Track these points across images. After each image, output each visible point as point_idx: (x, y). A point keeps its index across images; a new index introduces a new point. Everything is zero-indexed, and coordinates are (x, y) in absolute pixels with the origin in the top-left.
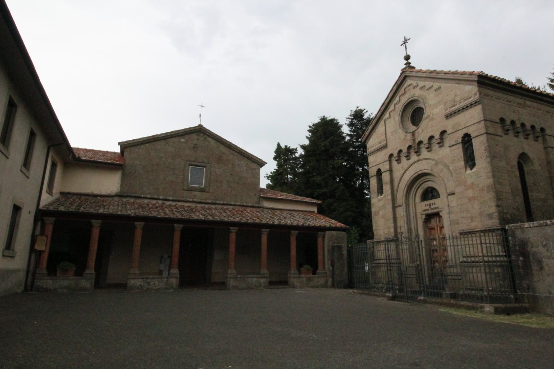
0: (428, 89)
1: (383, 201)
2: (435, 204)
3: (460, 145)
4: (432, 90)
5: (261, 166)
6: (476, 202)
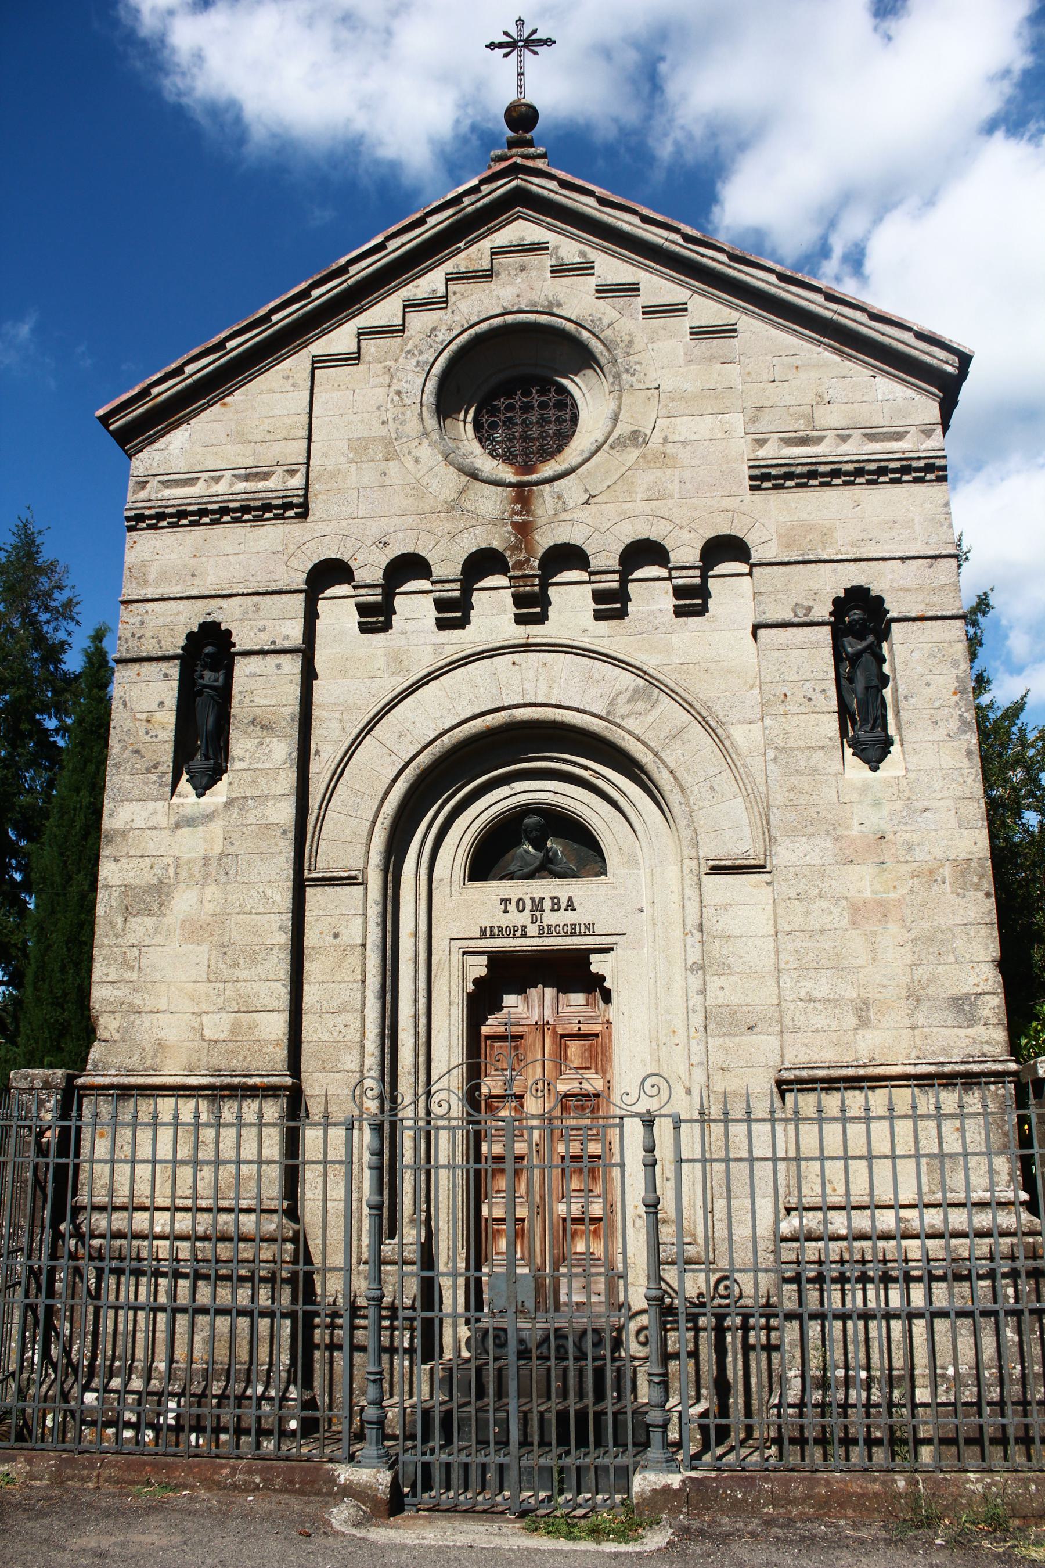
0: (649, 312)
1: (217, 827)
2: (571, 906)
3: (824, 634)
4: (684, 323)
6: (893, 928)
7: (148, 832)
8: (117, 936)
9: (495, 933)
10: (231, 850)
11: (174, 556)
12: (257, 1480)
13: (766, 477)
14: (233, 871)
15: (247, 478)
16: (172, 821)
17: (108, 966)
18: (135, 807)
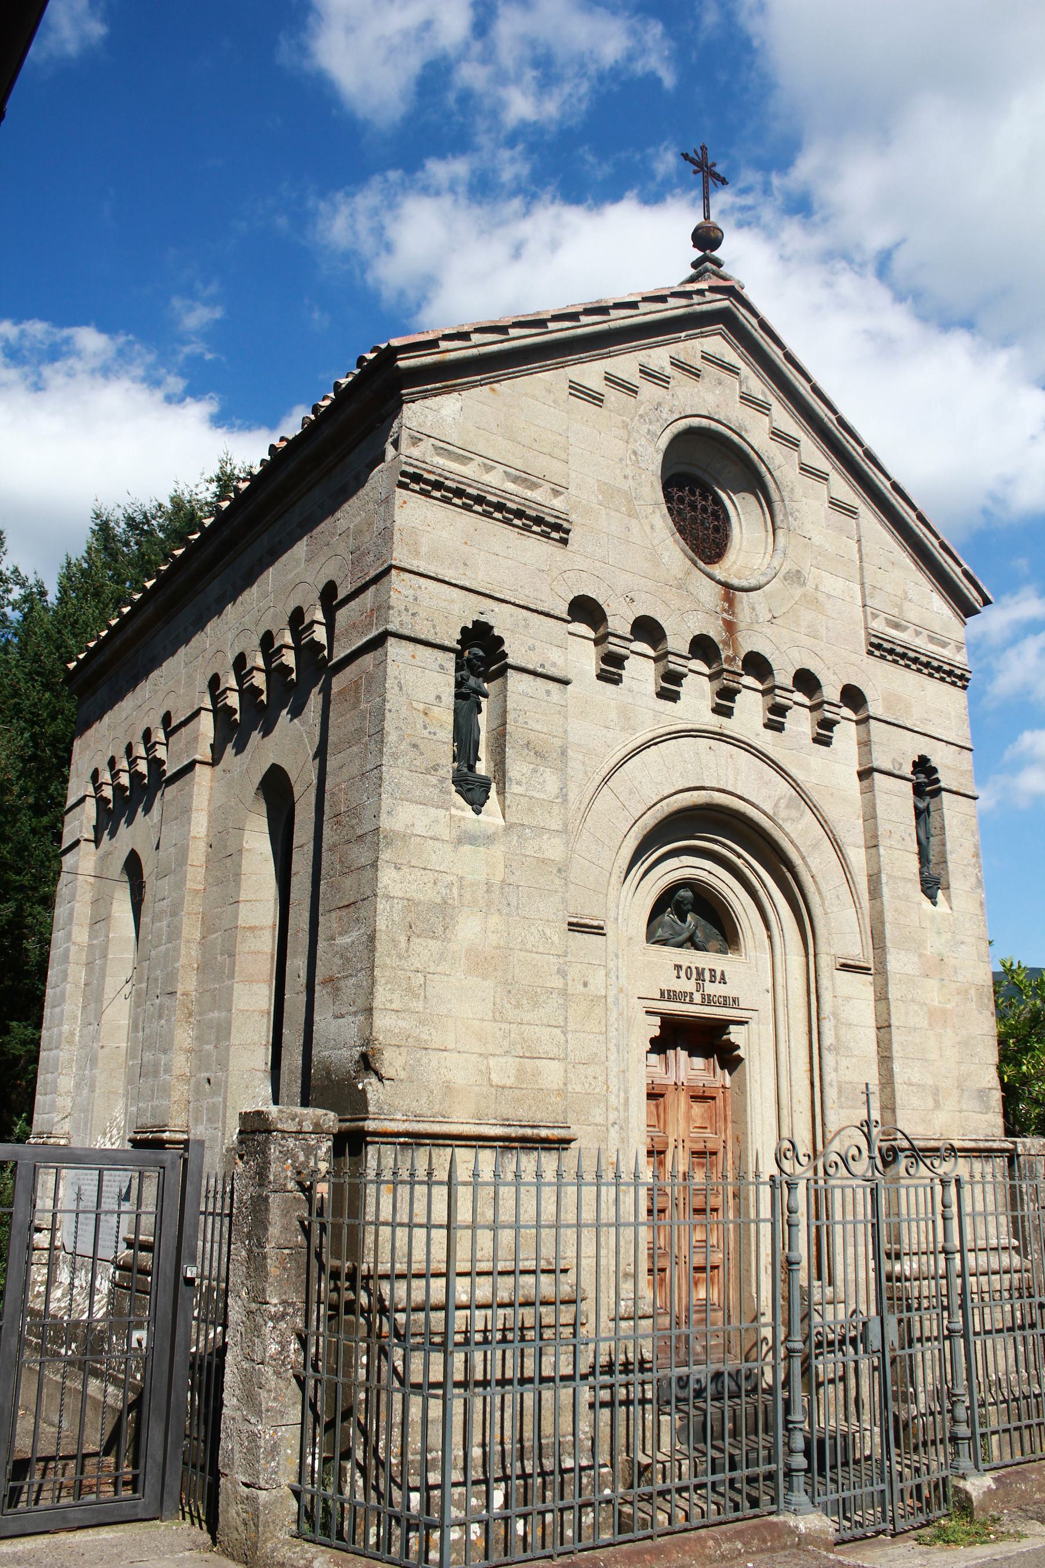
1: (498, 851)
2: (723, 980)
7: (430, 842)
8: (400, 957)
9: (668, 995)
10: (512, 879)
11: (445, 534)
12: (740, 1546)
13: (879, 647)
14: (514, 903)
15: (515, 480)
16: (454, 834)
17: (392, 991)
18: (415, 809)
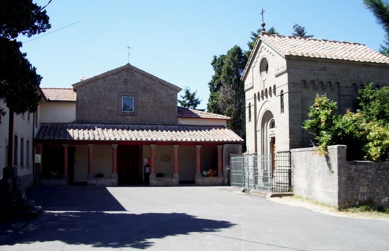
5: (178, 92)
